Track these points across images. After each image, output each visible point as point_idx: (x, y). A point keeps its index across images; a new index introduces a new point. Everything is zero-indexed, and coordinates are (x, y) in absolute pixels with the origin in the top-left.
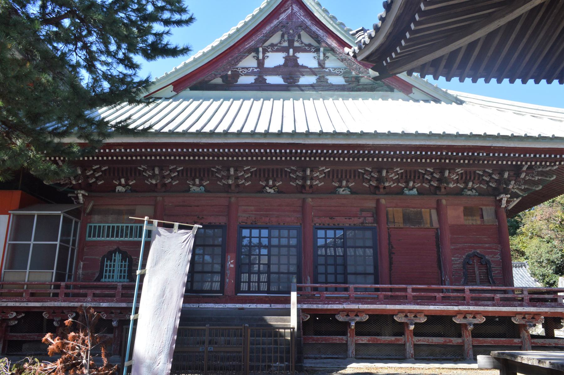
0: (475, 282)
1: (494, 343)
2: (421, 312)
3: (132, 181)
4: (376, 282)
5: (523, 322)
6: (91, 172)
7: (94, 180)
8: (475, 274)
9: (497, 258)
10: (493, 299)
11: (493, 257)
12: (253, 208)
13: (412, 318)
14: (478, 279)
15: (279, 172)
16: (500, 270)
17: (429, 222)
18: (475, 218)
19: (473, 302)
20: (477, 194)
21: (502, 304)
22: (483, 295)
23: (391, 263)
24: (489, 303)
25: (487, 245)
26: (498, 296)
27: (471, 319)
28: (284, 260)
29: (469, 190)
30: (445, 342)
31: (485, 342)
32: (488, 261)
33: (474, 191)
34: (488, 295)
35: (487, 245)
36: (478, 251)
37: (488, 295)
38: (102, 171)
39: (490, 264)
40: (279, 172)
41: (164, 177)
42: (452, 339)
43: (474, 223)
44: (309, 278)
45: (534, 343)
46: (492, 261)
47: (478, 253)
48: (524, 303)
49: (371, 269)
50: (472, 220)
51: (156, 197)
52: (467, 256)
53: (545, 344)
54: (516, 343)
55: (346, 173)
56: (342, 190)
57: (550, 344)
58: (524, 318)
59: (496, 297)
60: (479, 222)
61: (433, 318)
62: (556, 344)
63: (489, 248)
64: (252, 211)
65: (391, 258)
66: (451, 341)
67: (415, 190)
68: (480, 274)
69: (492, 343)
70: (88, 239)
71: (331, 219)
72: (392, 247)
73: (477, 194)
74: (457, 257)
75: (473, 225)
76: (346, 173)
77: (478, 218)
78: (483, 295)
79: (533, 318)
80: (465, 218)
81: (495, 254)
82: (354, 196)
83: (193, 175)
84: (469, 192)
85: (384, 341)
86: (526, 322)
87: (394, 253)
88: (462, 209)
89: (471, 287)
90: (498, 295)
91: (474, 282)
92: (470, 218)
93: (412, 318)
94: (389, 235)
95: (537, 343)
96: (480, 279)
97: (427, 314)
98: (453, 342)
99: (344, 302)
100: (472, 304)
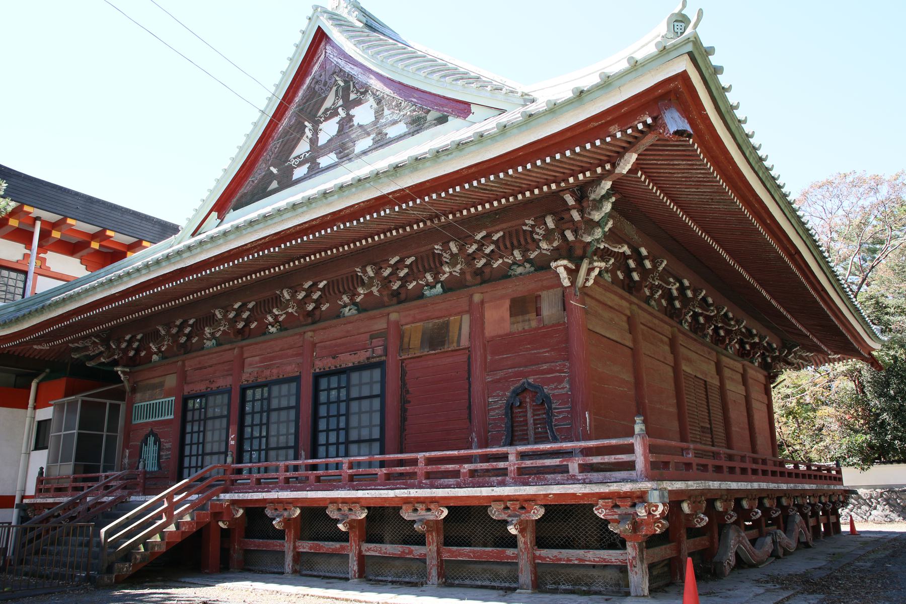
0: (527, 439)
1: (474, 557)
2: (356, 501)
3: (411, 282)
4: (382, 452)
5: (503, 516)
6: (475, 247)
7: (483, 261)
8: (526, 425)
9: (563, 388)
10: (456, 474)
11: (556, 388)
12: (257, 358)
13: (347, 512)
14: (531, 433)
15: (514, 235)
16: (568, 412)
17: (456, 339)
18: (527, 317)
19: (428, 481)
20: (533, 269)
21: (472, 482)
22: (443, 467)
23: (404, 419)
24: (452, 481)
25: (545, 367)
26: (467, 467)
27: (423, 513)
28: (283, 430)
29: (519, 266)
30: (403, 552)
31: (460, 555)
32: (547, 397)
33: (528, 265)
34: (450, 467)
35: (545, 367)
36: (531, 380)
37: (450, 467)
38: (493, 242)
39: (550, 403)
40: (514, 235)
41: (472, 257)
42: (413, 547)
43: (527, 327)
44: (303, 453)
45: (540, 557)
46: (554, 395)
47: (529, 384)
48: (508, 478)
49: (376, 434)
50: (523, 321)
51: (388, 314)
52: (514, 392)
53: (560, 559)
54: (508, 557)
55: (348, 280)
56: (347, 309)
57: (569, 560)
58: (507, 508)
59: (462, 470)
60: (534, 324)
61: (461, 513)
62: (580, 560)
63: (550, 371)
64: (257, 363)
65: (404, 410)
66: (411, 552)
67: (439, 286)
68: (535, 424)
69: (469, 556)
70: (134, 422)
71: (334, 358)
72: (407, 392)
73: (533, 269)
74: (498, 396)
75: (524, 331)
76: (348, 280)
77: (533, 316)
78: (443, 467)
79: (522, 508)
80: (513, 319)
81: (560, 380)
82: (363, 315)
83: (508, 245)
84: (520, 270)
85: (327, 549)
86: (509, 516)
87: (409, 402)
88: (507, 304)
89: (427, 454)
90: (466, 466)
91: (525, 441)
92: (520, 318)
93: (347, 512)
94: (404, 373)
95: (544, 558)
96: (535, 434)
97: (364, 503)
98: (415, 553)
99: (273, 489)
100: (426, 484)
